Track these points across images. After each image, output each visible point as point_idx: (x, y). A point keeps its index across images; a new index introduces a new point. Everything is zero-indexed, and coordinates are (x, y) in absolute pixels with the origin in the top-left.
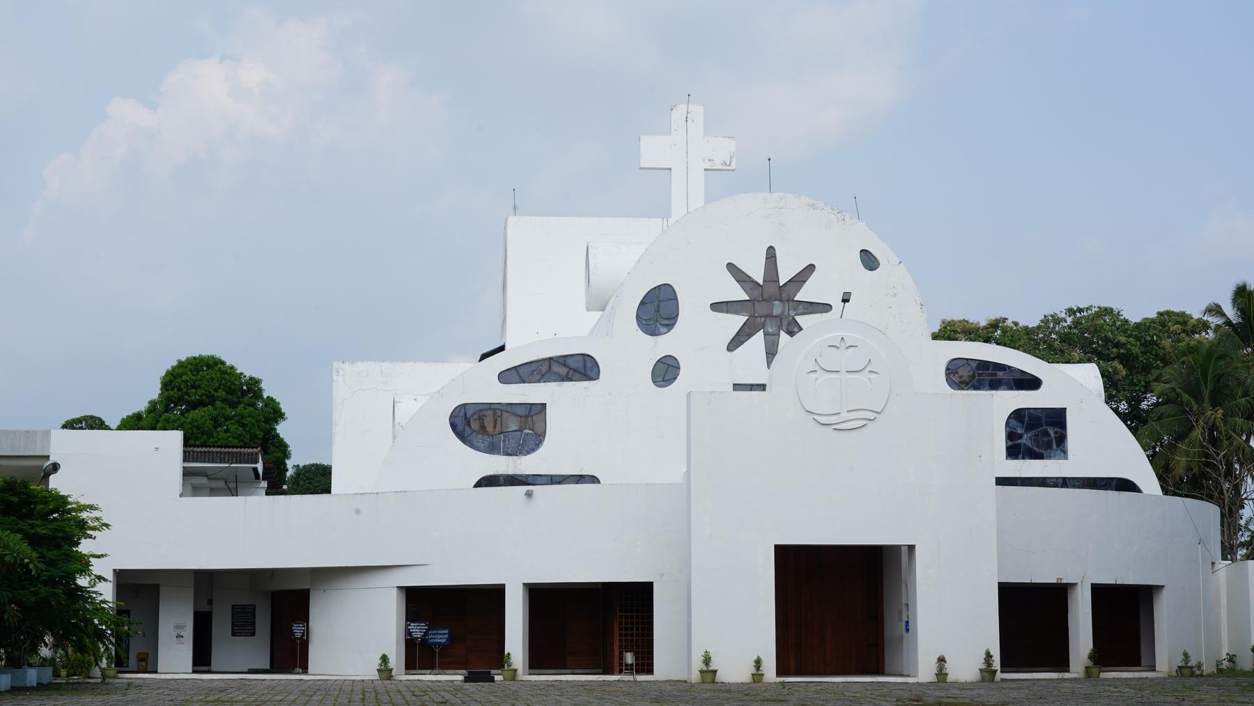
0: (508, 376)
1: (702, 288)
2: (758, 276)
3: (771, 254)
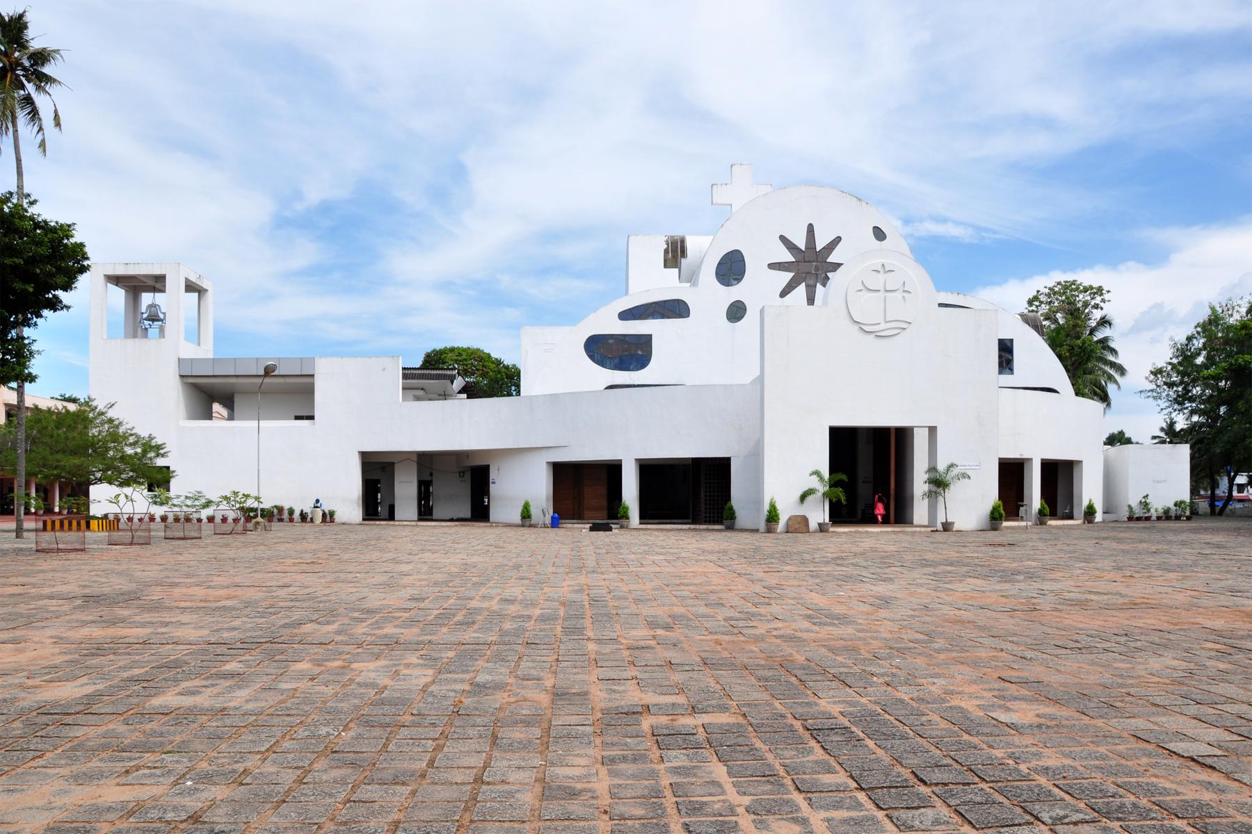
0: (625, 315)
1: (762, 252)
2: (802, 245)
3: (811, 229)
